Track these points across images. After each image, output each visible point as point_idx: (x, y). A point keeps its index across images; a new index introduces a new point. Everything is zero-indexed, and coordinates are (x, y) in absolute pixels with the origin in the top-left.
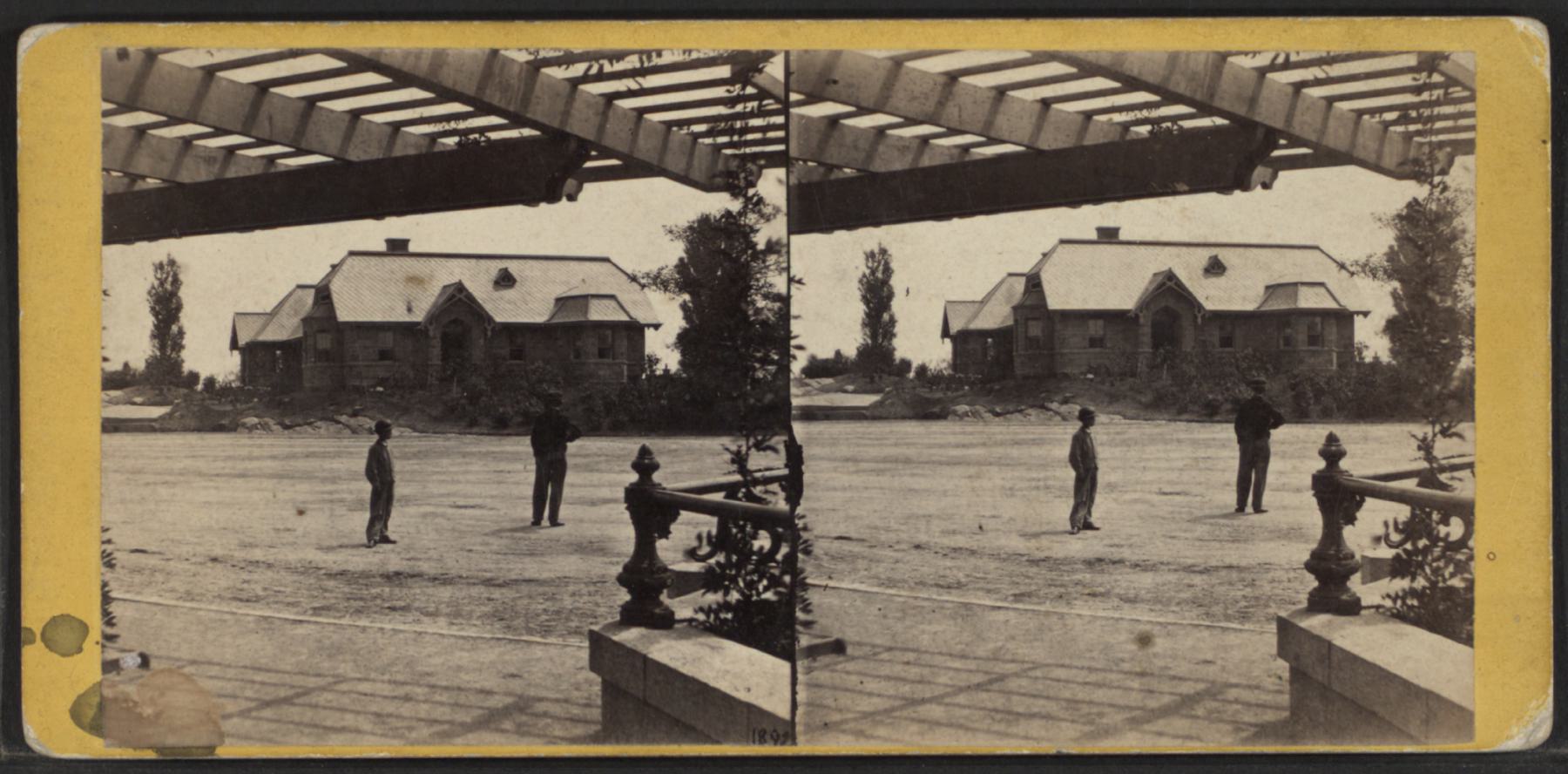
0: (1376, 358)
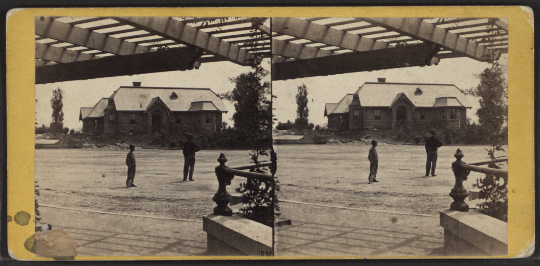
0: (474, 123)
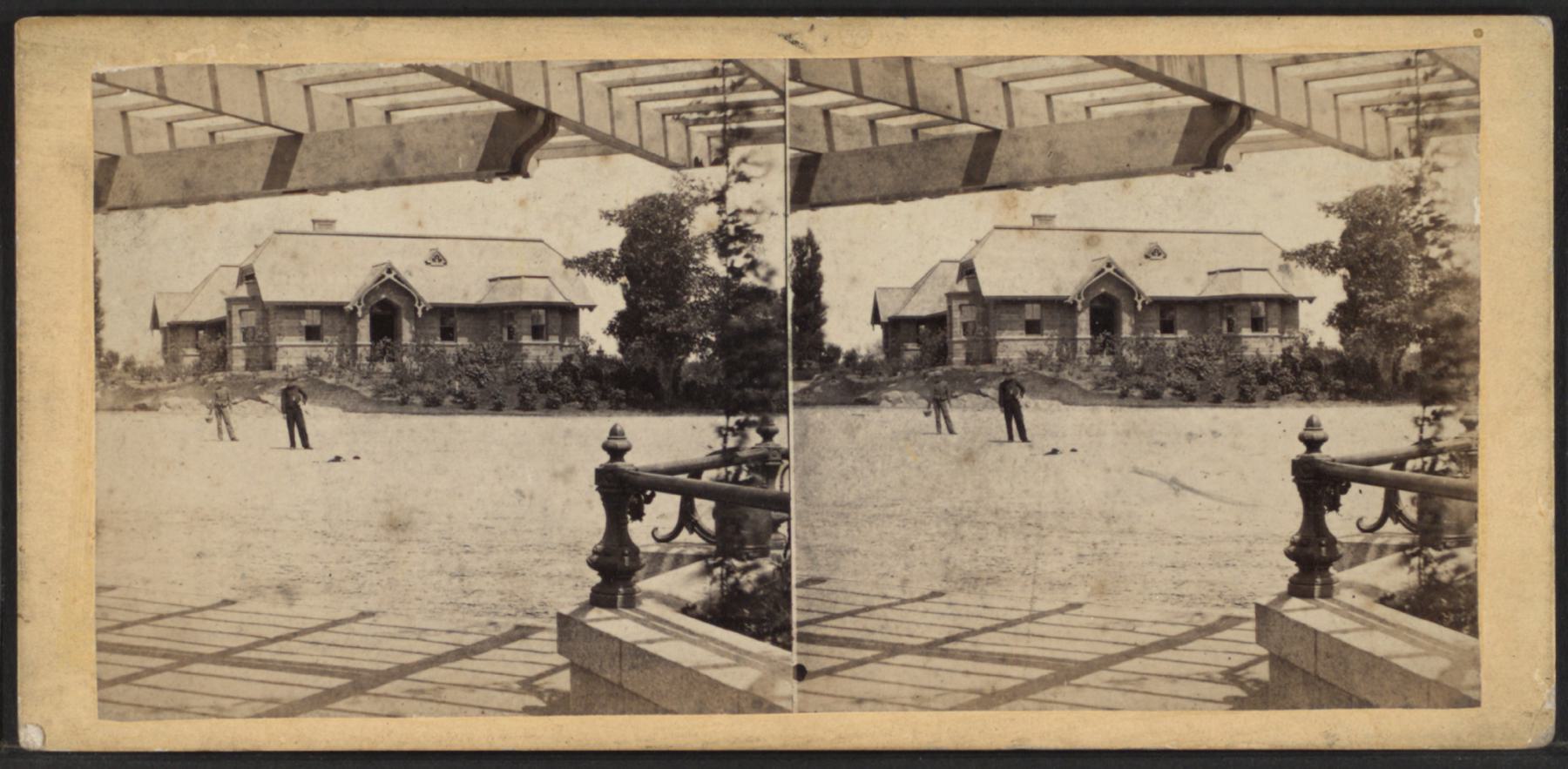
0: (600, 352)
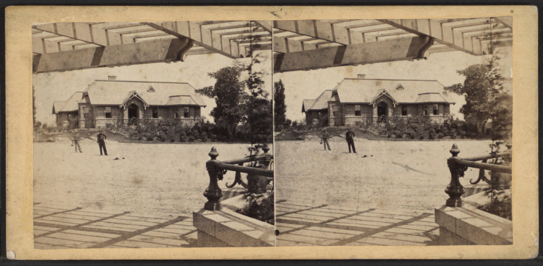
0: (208, 122)
